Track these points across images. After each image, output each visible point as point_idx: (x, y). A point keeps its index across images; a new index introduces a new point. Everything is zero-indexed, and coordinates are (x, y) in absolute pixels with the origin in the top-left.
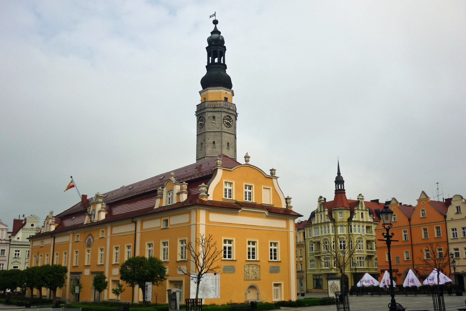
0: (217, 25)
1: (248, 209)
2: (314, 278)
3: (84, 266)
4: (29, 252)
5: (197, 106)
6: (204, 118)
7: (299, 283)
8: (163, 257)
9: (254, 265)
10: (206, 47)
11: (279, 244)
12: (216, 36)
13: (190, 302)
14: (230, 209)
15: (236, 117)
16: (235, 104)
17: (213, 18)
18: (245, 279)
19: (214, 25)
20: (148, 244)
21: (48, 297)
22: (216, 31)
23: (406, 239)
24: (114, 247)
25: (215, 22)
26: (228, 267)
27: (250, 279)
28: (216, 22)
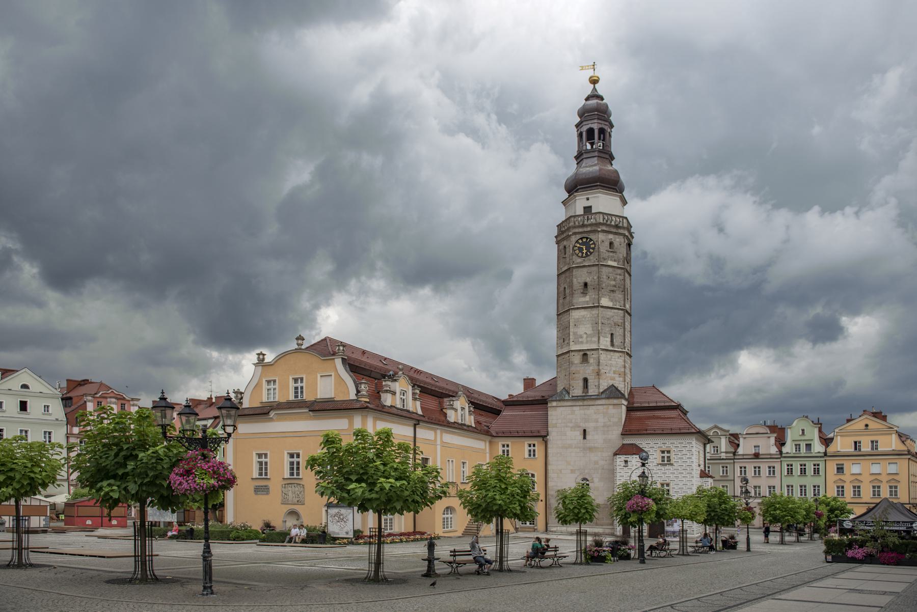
0: (596, 85)
2: (778, 539)
3: (251, 479)
4: (853, 464)
5: (557, 226)
8: (300, 470)
9: (296, 485)
10: (575, 124)
11: (467, 463)
12: (593, 102)
15: (631, 239)
16: (626, 218)
17: (590, 73)
18: (283, 503)
19: (593, 85)
22: (594, 96)
23: (725, 471)
24: (254, 454)
25: (594, 81)
26: (260, 488)
27: (290, 503)
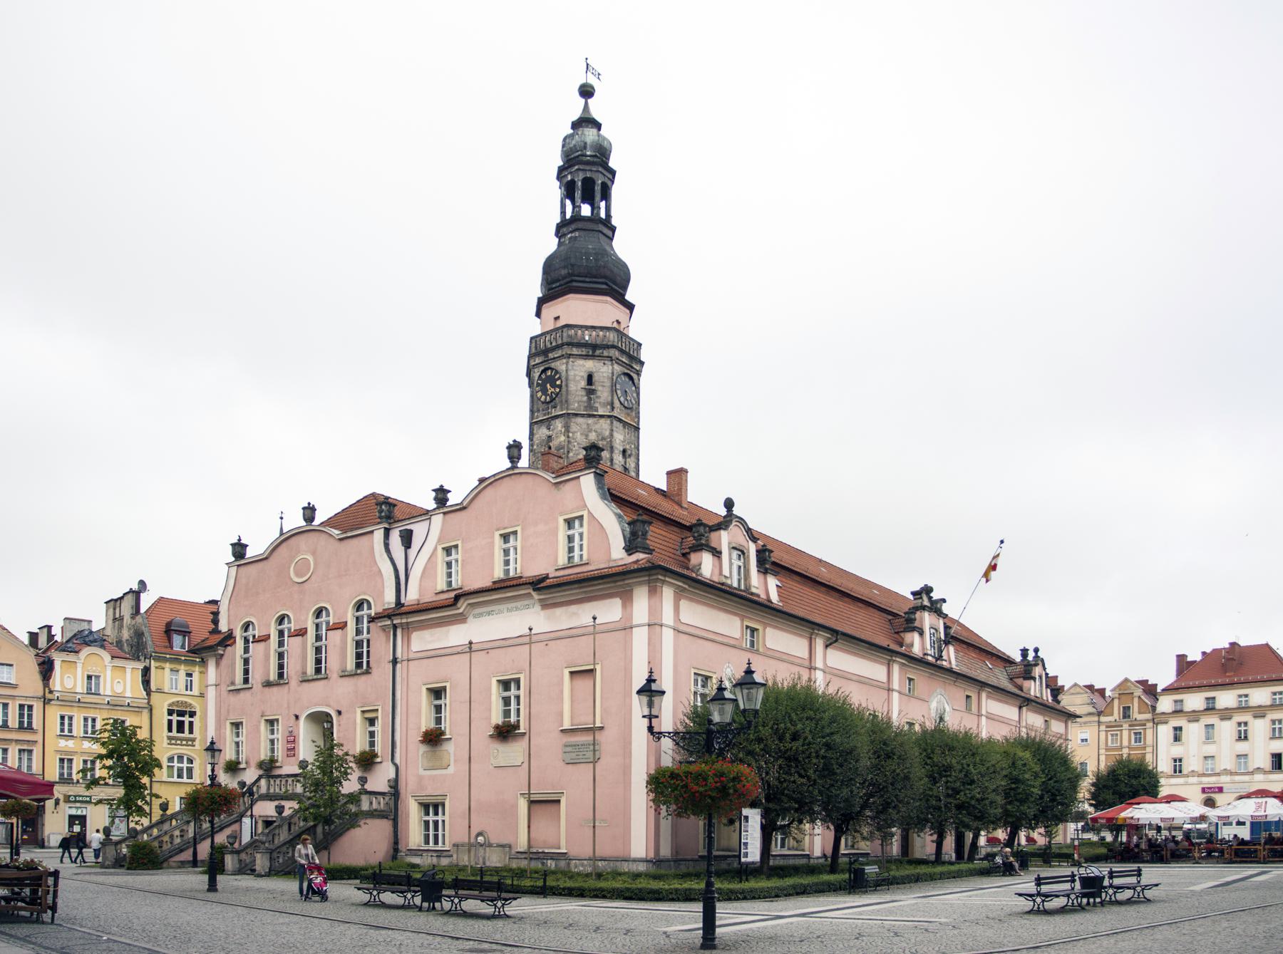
0: (589, 101)
1: (676, 580)
6: (557, 372)
7: (60, 902)
13: (1127, 744)
14: (519, 604)
19: (584, 100)
20: (498, 681)
21: (984, 695)
22: (586, 122)
25: (586, 92)
28: (590, 89)
